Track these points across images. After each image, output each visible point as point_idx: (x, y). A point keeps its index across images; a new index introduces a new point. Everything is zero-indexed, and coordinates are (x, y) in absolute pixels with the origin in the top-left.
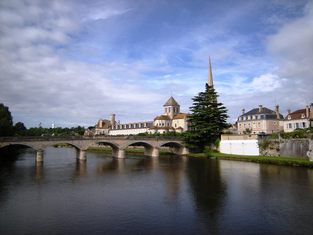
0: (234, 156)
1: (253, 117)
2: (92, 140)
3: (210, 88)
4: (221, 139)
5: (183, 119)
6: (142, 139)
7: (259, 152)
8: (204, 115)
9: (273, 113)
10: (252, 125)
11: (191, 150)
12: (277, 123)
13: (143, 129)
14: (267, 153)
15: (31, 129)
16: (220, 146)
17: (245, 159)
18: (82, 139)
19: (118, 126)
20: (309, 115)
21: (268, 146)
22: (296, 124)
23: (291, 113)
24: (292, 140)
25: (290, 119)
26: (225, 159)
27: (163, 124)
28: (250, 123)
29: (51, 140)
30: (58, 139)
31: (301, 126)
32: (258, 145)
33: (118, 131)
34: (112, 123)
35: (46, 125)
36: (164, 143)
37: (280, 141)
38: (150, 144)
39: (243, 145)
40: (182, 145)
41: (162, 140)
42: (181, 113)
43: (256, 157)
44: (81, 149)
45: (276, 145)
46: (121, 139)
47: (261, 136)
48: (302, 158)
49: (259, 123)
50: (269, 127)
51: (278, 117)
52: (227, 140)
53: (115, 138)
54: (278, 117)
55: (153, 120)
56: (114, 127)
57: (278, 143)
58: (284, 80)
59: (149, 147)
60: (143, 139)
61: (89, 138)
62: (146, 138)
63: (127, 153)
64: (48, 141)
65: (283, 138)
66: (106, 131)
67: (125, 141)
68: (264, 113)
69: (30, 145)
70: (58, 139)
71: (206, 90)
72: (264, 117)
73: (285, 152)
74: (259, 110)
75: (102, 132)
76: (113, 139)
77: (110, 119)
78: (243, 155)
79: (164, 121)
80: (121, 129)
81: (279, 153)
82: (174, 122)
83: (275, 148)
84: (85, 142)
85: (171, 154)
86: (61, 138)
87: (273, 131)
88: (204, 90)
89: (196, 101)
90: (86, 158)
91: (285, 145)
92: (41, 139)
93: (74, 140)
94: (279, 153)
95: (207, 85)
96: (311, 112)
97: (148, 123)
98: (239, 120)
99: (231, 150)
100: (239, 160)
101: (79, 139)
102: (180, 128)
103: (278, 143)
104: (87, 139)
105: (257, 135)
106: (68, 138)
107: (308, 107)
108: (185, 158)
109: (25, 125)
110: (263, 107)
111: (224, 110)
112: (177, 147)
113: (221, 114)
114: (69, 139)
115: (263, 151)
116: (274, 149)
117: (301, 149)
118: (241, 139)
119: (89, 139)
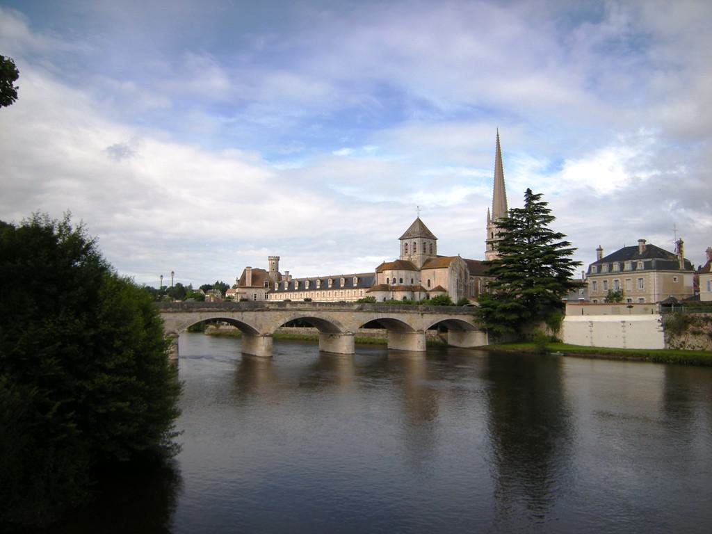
1: (614, 266)
4: (567, 312)
5: (446, 269)
7: (665, 340)
10: (623, 282)
11: (493, 335)
14: (684, 343)
16: (564, 328)
21: (686, 328)
23: (603, 257)
27: (401, 281)
28: (619, 279)
29: (195, 310)
30: (210, 309)
32: (662, 326)
34: (273, 275)
36: (437, 320)
38: (406, 322)
41: (432, 313)
42: (438, 256)
44: (261, 332)
45: (707, 325)
46: (345, 311)
47: (670, 305)
51: (682, 266)
53: (332, 308)
54: (682, 266)
55: (374, 271)
56: (280, 285)
60: (392, 312)
61: (277, 307)
63: (359, 344)
67: (355, 315)
68: (653, 258)
70: (210, 309)
71: (525, 203)
72: (653, 265)
74: (638, 251)
76: (330, 310)
79: (403, 273)
82: (426, 274)
83: (706, 332)
86: (217, 307)
95: (529, 191)
98: (592, 271)
99: (591, 338)
102: (440, 289)
104: (274, 310)
105: (657, 305)
106: (232, 307)
110: (647, 243)
111: (564, 248)
112: (459, 327)
113: (561, 257)
114: (233, 309)
115: (674, 338)
116: (703, 334)
119: (277, 310)
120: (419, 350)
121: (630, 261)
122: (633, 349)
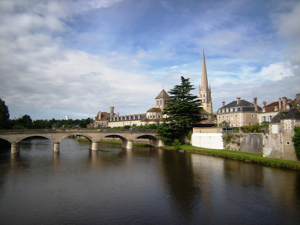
0: (199, 150)
1: (231, 109)
2: (65, 133)
3: (186, 81)
6: (116, 131)
7: (223, 145)
8: (177, 109)
9: (251, 105)
11: (166, 143)
12: (254, 116)
13: (137, 121)
15: (38, 121)
17: (208, 153)
18: (55, 132)
19: (116, 118)
20: (282, 108)
22: (269, 117)
23: (267, 105)
24: (250, 135)
25: (264, 111)
26: (204, 154)
27: (154, 117)
29: (24, 133)
30: (31, 132)
31: (268, 119)
32: (222, 139)
33: (115, 123)
35: (59, 117)
36: (139, 135)
37: (241, 135)
39: (210, 139)
40: (157, 137)
43: (217, 151)
45: (237, 139)
46: (94, 132)
48: (259, 153)
49: (236, 116)
50: (246, 119)
51: (256, 109)
52: (199, 133)
54: (256, 109)
57: (239, 137)
58: (296, 67)
59: (124, 140)
60: (117, 132)
62: (120, 131)
64: (22, 134)
65: (244, 132)
66: (105, 122)
68: (241, 106)
69: (5, 138)
70: (31, 132)
71: (182, 83)
73: (244, 146)
75: (100, 124)
77: (109, 111)
78: (210, 148)
79: (155, 114)
80: (118, 121)
81: (239, 148)
84: (58, 134)
85: (150, 146)
86: (35, 131)
87: (250, 124)
88: (180, 83)
89: (173, 94)
90: (59, 150)
91: (245, 139)
92: (15, 132)
93: (47, 133)
94: (239, 148)
95: (182, 78)
96: (283, 105)
97: (142, 115)
98: (219, 112)
100: (203, 153)
101: (52, 132)
103: (239, 137)
104: (60, 132)
107: (281, 99)
108: (160, 151)
109: (31, 117)
110: (241, 99)
114: (42, 132)
117: (258, 144)
118: (215, 132)
119: (62, 132)
120: (130, 148)
121: (232, 108)
122: (215, 150)
